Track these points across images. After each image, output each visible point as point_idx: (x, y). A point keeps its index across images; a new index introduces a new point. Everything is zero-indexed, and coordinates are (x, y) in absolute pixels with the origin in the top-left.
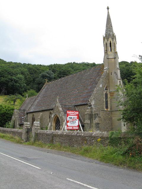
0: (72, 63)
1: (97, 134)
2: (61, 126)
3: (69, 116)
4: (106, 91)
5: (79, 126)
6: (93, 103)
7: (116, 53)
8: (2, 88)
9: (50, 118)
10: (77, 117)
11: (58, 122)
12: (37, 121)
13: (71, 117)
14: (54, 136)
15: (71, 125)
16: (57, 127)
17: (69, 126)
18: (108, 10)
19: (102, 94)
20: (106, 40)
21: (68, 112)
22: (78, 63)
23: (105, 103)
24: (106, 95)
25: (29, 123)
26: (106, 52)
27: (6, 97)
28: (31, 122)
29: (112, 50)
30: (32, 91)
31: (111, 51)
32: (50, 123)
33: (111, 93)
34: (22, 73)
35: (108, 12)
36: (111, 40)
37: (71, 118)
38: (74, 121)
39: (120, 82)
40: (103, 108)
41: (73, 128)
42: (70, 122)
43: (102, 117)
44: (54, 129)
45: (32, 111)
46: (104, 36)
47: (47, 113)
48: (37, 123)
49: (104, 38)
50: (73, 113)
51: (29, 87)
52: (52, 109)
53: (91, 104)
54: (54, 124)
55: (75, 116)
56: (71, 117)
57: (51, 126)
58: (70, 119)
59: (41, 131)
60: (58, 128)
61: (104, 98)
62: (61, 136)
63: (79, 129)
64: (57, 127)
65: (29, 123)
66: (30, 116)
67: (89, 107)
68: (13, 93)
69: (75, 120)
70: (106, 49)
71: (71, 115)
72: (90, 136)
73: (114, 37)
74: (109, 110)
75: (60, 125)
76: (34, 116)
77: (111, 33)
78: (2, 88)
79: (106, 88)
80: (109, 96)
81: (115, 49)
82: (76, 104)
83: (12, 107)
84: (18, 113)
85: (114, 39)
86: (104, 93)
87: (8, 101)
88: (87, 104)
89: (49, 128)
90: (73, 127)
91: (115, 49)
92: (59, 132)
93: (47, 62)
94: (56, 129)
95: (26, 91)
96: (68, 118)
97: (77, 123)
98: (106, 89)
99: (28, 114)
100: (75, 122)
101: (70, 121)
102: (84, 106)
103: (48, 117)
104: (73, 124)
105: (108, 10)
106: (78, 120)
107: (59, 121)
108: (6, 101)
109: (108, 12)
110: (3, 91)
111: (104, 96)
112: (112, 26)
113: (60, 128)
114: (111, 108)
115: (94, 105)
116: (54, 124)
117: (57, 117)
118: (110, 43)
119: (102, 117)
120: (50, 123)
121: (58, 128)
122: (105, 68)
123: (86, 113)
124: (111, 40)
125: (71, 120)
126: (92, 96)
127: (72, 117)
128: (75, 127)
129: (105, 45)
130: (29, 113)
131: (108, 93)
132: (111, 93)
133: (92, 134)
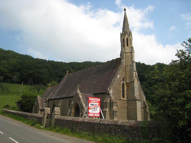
0: (88, 61)
1: (123, 122)
2: (80, 113)
3: (91, 103)
4: (123, 81)
5: (100, 113)
6: (111, 92)
7: (132, 48)
8: (29, 79)
9: (69, 105)
10: (98, 104)
11: (77, 109)
12: (57, 107)
13: (93, 103)
14: (73, 122)
15: (93, 112)
16: (76, 113)
17: (90, 113)
18: (125, 11)
19: (120, 84)
20: (123, 36)
21: (90, 99)
22: (93, 62)
23: (122, 93)
24: (123, 85)
25: (49, 109)
26: (123, 46)
27: (33, 87)
28: (52, 108)
29: (129, 45)
30: (54, 82)
31: (127, 46)
32: (70, 110)
33: (127, 83)
34: (46, 68)
35: (125, 13)
36: (128, 37)
37: (93, 105)
38: (96, 108)
39: (136, 74)
40: (120, 97)
41: (94, 115)
42: (92, 109)
43: (119, 105)
44: (74, 116)
45: (53, 98)
46: (121, 33)
47: (68, 100)
48: (57, 109)
49: (121, 35)
50: (95, 100)
51: (52, 79)
52: (72, 97)
53: (110, 92)
54: (73, 111)
55: (96, 103)
56: (93, 103)
57: (71, 112)
58: (91, 106)
59: (62, 117)
60: (77, 115)
61: (121, 88)
62: (83, 123)
63: (101, 117)
64: (76, 113)
65: (49, 109)
66: (52, 102)
67: (107, 96)
68: (38, 83)
69: (97, 107)
70: (123, 44)
71: (93, 101)
72: (114, 125)
73: (130, 34)
74: (125, 99)
75: (79, 112)
76: (54, 102)
77: (128, 30)
78: (29, 79)
79: (123, 78)
80: (125, 86)
81: (131, 44)
82: (95, 93)
83: (35, 94)
84: (41, 100)
85: (131, 36)
86: (122, 83)
87: (33, 90)
88: (105, 93)
89: (68, 114)
90: (94, 114)
91: (131, 44)
92: (80, 119)
93: (67, 61)
94: (75, 116)
95: (49, 82)
96: (90, 104)
97: (98, 110)
98: (123, 80)
99: (50, 101)
100: (96, 109)
101: (92, 108)
102: (102, 95)
103: (68, 104)
104: (95, 111)
105: (125, 11)
106: (99, 107)
107: (79, 108)
108: (32, 90)
109: (125, 13)
110: (30, 81)
111: (121, 86)
112: (128, 25)
113: (79, 115)
114: (127, 98)
115: (112, 94)
116: (74, 111)
117: (76, 104)
118: (127, 39)
119: (119, 105)
120: (70, 110)
121: (77, 115)
122: (122, 61)
123: (104, 101)
124: (128, 37)
125: (92, 107)
126: (110, 85)
127: (94, 104)
128: (96, 114)
129: (123, 41)
130: (50, 100)
131: (125, 83)
132: (127, 83)
133: (117, 122)
